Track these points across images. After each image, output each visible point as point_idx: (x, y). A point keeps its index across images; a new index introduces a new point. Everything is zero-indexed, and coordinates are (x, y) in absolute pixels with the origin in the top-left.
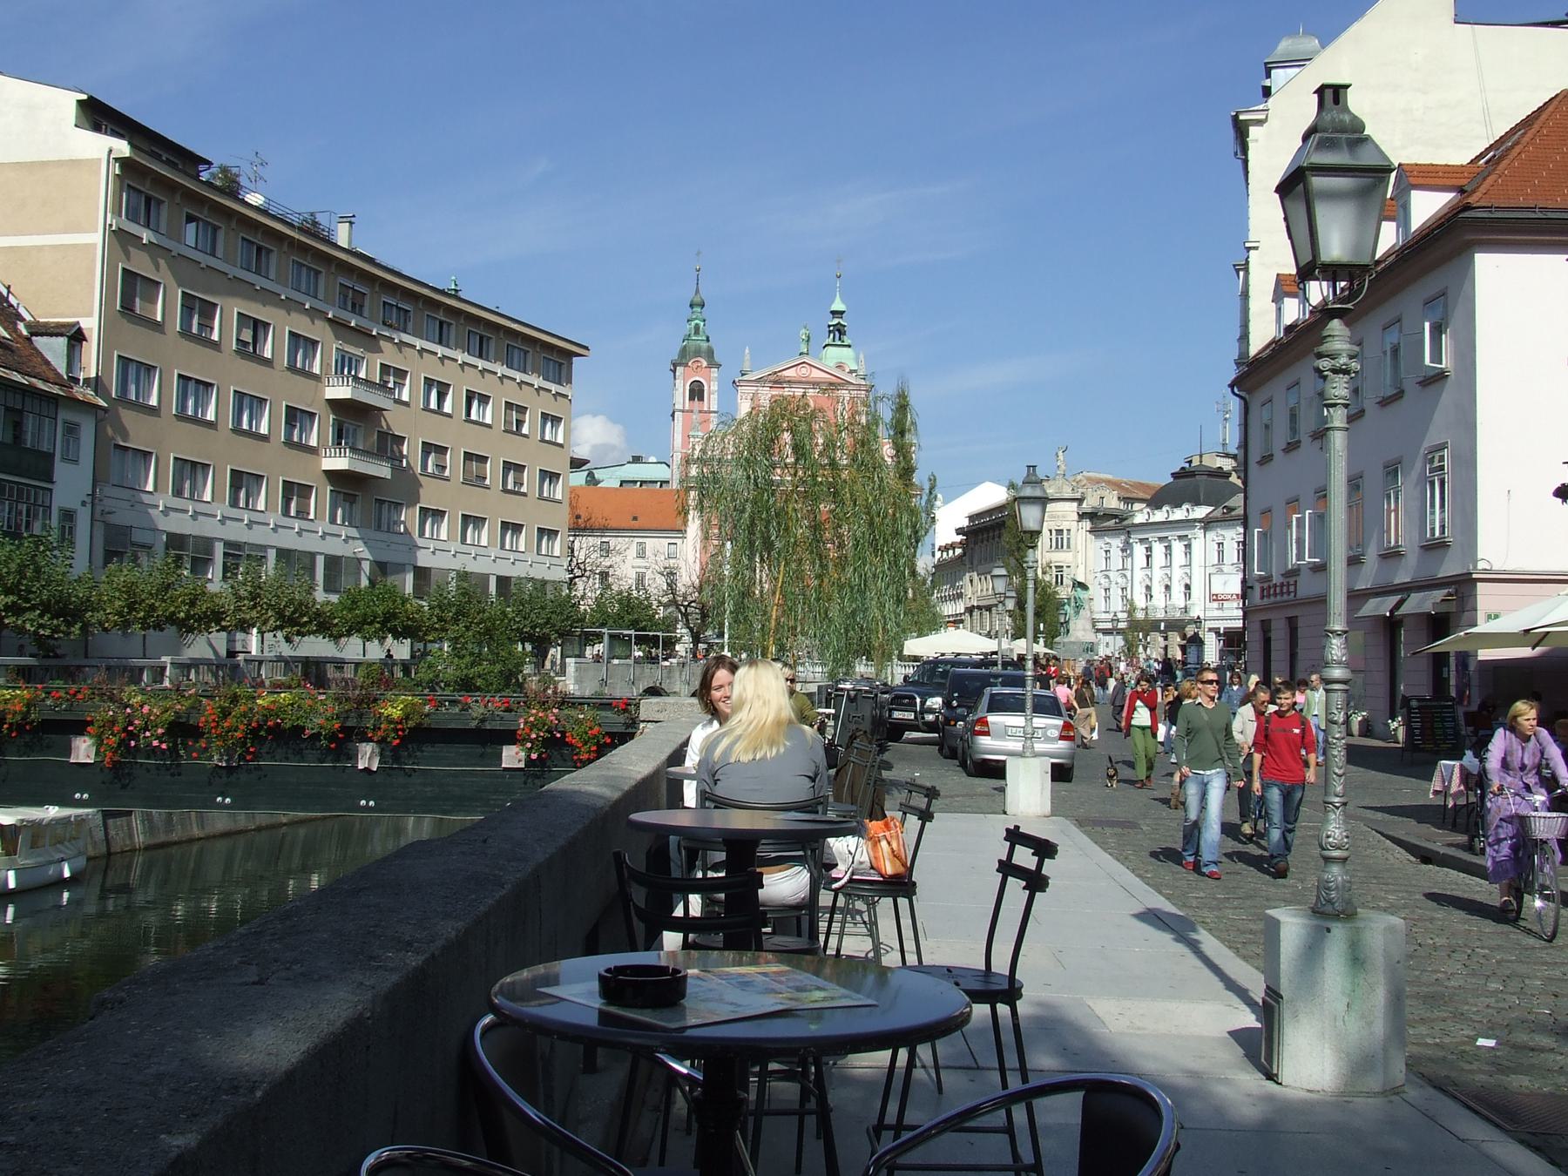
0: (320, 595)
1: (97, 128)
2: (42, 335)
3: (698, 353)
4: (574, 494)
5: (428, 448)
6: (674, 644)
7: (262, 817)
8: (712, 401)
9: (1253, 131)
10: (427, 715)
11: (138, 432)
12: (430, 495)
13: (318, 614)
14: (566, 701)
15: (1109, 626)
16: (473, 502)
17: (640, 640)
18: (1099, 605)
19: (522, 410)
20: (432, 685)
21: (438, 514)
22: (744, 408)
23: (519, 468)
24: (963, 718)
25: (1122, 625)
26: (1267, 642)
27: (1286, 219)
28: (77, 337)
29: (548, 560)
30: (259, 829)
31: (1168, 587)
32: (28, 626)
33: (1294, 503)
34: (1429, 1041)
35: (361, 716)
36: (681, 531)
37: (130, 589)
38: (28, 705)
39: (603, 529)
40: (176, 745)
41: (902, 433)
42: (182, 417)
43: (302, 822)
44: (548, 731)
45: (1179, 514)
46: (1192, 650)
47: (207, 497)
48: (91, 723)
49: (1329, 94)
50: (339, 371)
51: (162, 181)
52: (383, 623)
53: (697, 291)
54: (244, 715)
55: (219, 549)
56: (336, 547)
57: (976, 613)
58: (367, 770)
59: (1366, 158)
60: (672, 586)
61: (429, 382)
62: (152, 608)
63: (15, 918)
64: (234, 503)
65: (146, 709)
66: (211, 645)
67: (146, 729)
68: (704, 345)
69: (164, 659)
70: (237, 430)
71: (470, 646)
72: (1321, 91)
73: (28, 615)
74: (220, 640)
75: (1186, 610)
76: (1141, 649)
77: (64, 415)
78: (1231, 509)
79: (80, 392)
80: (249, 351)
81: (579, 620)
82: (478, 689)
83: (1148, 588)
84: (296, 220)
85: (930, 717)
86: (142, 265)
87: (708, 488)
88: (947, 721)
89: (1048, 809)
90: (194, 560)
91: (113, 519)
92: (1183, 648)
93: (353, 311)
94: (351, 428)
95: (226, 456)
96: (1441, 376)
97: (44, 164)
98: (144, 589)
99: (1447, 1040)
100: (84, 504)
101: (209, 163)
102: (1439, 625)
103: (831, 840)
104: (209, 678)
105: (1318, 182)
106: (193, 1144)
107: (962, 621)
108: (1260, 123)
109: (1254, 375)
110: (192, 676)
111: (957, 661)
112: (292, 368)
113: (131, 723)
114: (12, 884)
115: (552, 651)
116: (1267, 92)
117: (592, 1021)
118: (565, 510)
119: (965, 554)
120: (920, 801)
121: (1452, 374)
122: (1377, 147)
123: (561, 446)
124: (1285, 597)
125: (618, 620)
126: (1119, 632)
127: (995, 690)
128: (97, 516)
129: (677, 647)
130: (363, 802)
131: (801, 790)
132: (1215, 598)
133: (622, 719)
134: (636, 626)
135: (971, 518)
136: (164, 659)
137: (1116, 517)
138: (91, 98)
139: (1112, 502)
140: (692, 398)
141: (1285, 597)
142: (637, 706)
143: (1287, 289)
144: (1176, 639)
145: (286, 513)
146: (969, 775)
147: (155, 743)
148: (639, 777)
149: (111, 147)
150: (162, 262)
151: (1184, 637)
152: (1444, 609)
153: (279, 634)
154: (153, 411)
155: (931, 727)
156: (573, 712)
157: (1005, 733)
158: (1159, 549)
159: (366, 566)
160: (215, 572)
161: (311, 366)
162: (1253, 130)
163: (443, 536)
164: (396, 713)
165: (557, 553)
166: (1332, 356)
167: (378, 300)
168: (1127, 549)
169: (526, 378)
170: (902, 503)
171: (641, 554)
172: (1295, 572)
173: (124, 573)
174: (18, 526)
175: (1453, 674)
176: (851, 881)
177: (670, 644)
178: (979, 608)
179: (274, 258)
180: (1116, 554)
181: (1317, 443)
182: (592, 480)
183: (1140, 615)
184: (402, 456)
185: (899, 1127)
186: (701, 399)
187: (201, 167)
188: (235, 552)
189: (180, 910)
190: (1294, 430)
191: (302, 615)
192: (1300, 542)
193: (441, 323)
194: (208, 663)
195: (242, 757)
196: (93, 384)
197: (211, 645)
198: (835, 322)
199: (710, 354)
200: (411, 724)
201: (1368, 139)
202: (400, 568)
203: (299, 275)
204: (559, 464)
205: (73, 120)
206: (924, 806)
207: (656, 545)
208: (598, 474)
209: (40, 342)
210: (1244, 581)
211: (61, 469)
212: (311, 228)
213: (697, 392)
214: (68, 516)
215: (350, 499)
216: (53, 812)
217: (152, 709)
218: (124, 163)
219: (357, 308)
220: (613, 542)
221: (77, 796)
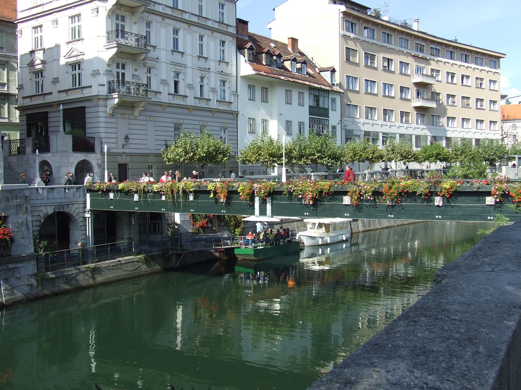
0: (414, 149)
2: (323, 71)
7: (399, 222)
10: (459, 187)
11: (354, 99)
23: (482, 100)
30: (398, 226)
35: (435, 188)
37: (354, 150)
40: (375, 198)
42: (367, 93)
48: (349, 192)
52: (436, 157)
55: (381, 135)
56: (419, 132)
58: (438, 206)
61: (448, 73)
63: (330, 251)
64: (385, 120)
65: (365, 187)
67: (365, 193)
70: (384, 96)
71: (466, 164)
73: (324, 159)
74: (383, 165)
77: (331, 96)
79: (336, 88)
80: (387, 69)
81: (507, 153)
84: (399, 24)
86: (351, 45)
90: (373, 139)
91: (348, 128)
94: (422, 91)
98: (358, 149)
100: (338, 123)
101: (370, 9)
112: (401, 73)
113: (361, 192)
128: (343, 127)
147: (369, 198)
150: (358, 44)
153: (402, 162)
154: (358, 92)
159: (429, 138)
160: (380, 142)
164: (448, 186)
173: (351, 145)
179: (393, 37)
182: (508, 102)
184: (440, 100)
187: (368, 11)
188: (386, 136)
189: (373, 252)
191: (409, 155)
193: (451, 52)
194: (380, 172)
195: (396, 202)
200: (453, 190)
202: (441, 138)
203: (402, 42)
204: (496, 97)
205: (328, 2)
208: (510, 100)
211: (331, 113)
212: (405, 26)
214: (334, 128)
215: (423, 116)
217: (368, 187)
218: (344, 13)
219: (422, 50)
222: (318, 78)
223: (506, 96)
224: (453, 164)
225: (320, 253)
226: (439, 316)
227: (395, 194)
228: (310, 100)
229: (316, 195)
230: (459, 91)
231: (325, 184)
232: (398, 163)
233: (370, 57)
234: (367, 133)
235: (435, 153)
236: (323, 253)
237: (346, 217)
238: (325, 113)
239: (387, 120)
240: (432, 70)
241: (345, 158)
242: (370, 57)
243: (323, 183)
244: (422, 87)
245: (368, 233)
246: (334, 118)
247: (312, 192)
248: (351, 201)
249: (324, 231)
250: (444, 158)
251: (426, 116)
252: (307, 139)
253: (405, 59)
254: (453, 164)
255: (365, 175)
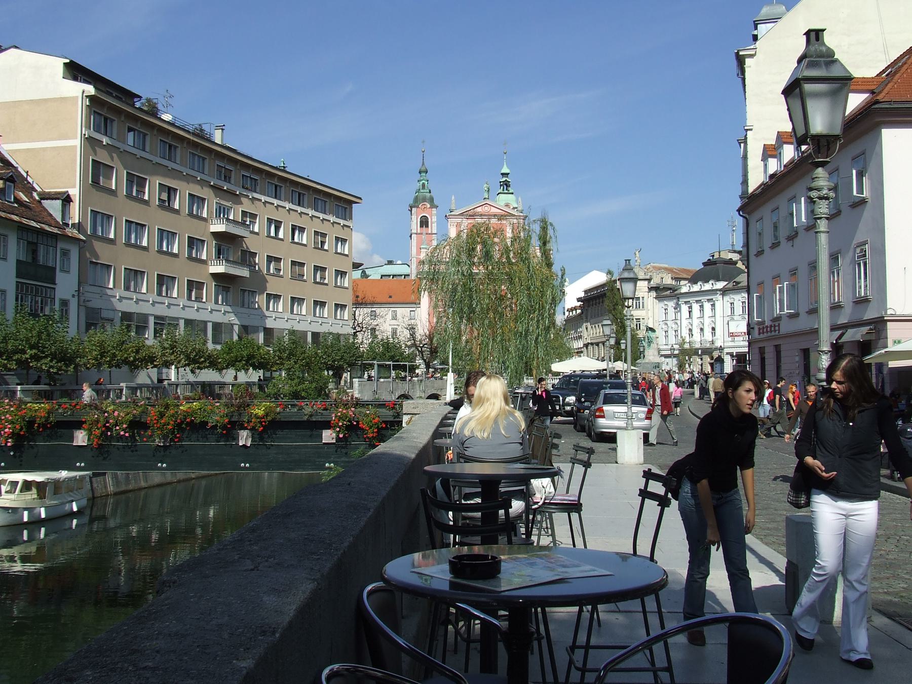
0: (210, 346)
1: (75, 79)
2: (47, 199)
3: (424, 200)
4: (355, 283)
5: (270, 259)
6: (415, 369)
7: (181, 475)
8: (433, 227)
9: (748, 61)
10: (279, 413)
11: (104, 253)
12: (273, 286)
13: (210, 356)
14: (358, 403)
15: (669, 353)
16: (297, 289)
17: (396, 367)
18: (662, 341)
19: (324, 235)
20: (276, 396)
21: (277, 297)
22: (453, 233)
23: (323, 269)
24: (588, 408)
25: (676, 352)
26: (763, 360)
27: (788, 109)
28: (67, 200)
29: (341, 322)
30: (179, 482)
31: (702, 330)
32: (44, 367)
33: (777, 278)
34: (880, 591)
35: (240, 414)
36: (417, 303)
37: (101, 344)
38: (49, 413)
39: (373, 304)
40: (134, 433)
41: (545, 244)
42: (128, 244)
43: (204, 477)
44: (349, 421)
45: (707, 287)
46: (717, 366)
47: (144, 290)
48: (85, 422)
49: (813, 35)
50: (218, 216)
51: (114, 108)
52: (247, 361)
53: (423, 164)
54: (173, 416)
55: (152, 320)
56: (218, 318)
57: (590, 347)
58: (244, 446)
59: (835, 72)
60: (413, 335)
61: (270, 221)
62: (114, 355)
63: (46, 535)
64: (160, 294)
65: (116, 413)
66: (150, 377)
67: (117, 425)
68: (428, 195)
69: (122, 384)
70: (160, 251)
71: (297, 373)
72: (808, 34)
73: (43, 361)
74: (153, 372)
75: (713, 342)
76: (687, 366)
77: (61, 245)
78: (738, 283)
79: (70, 232)
80: (166, 206)
81: (362, 356)
82: (303, 398)
83: (690, 330)
84: (191, 129)
85: (568, 408)
86: (103, 157)
87: (432, 277)
88: (579, 410)
89: (642, 460)
90: (137, 327)
91: (90, 305)
92: (712, 365)
93: (225, 180)
94: (226, 248)
95: (155, 266)
96: (863, 202)
97: (46, 101)
98: (110, 343)
99: (891, 590)
100: (73, 296)
101: (140, 97)
102: (866, 347)
103: (532, 481)
104: (148, 395)
105: (808, 87)
106: (252, 666)
107: (582, 352)
108: (752, 56)
109: (751, 204)
110: (138, 394)
111: (583, 375)
112: (191, 214)
113: (108, 422)
114: (43, 516)
115: (345, 375)
116: (755, 38)
117: (446, 587)
118: (350, 293)
119: (582, 313)
120: (584, 456)
121: (869, 200)
122: (842, 65)
123: (347, 255)
124: (773, 333)
125: (382, 356)
126: (675, 356)
127: (608, 391)
128: (81, 303)
129: (417, 371)
130: (243, 465)
131: (516, 450)
132: (732, 335)
133: (391, 413)
134: (392, 359)
135: (586, 292)
136: (122, 384)
137: (670, 289)
138: (71, 61)
139: (668, 281)
140: (421, 226)
141: (773, 333)
142: (401, 406)
143: (770, 153)
144: (707, 359)
145: (189, 298)
146: (593, 441)
147: (122, 433)
148: (421, 446)
149: (81, 90)
150: (115, 155)
151: (712, 358)
152: (868, 338)
153: (188, 369)
154: (112, 242)
155: (569, 414)
156: (363, 410)
157: (614, 416)
158: (696, 307)
159: (236, 328)
160: (149, 334)
161: (202, 213)
162: (748, 61)
163: (280, 310)
164: (260, 412)
165: (346, 318)
166: (818, 189)
167: (240, 174)
168: (677, 307)
169: (326, 217)
170: (546, 282)
171: (394, 318)
172: (779, 318)
173: (98, 336)
174: (36, 310)
175: (874, 376)
176: (544, 503)
177: (413, 369)
178: (592, 344)
179: (179, 151)
180: (671, 311)
181: (790, 243)
182: (364, 275)
183: (687, 346)
184: (256, 264)
185: (587, 647)
186: (427, 226)
187: (136, 100)
188: (161, 322)
189: (134, 530)
190: (776, 237)
191: (201, 357)
192: (781, 301)
193: (276, 186)
194: (147, 386)
195: (172, 440)
196: (77, 226)
197: (150, 377)
198: (504, 179)
199: (431, 200)
200: (269, 418)
201: (837, 61)
202: (256, 330)
203: (194, 159)
204: (346, 266)
205: (62, 75)
206: (586, 459)
207: (403, 312)
208: (368, 272)
209: (46, 203)
210: (748, 325)
211: (60, 276)
212: (200, 133)
213: (424, 223)
214: (65, 303)
215: (226, 290)
216: (64, 474)
217: (120, 414)
218: (91, 98)
219: (227, 179)
220: (378, 311)
221: (78, 464)
222: (38, 210)
223: (361, 265)
224: (276, 374)
225: (25, 538)
226: (119, 665)
227: (170, 427)
228: (18, 249)
229: (22, 429)
230: (288, 254)
231: (40, 408)
232: (181, 370)
233: (136, 182)
234: (127, 316)
235: (245, 353)
236: (31, 539)
237: (80, 469)
238: (49, 275)
239: (164, 294)
240: (244, 213)
241: (84, 360)
242: (136, 182)
243: (36, 406)
244: (226, 241)
245: (123, 497)
246: (66, 285)
247: (12, 423)
248: (89, 440)
249: (36, 496)
250: (260, 363)
251: (231, 290)
252: (10, 322)
253: (198, 191)
254: (276, 374)
255: (121, 390)
